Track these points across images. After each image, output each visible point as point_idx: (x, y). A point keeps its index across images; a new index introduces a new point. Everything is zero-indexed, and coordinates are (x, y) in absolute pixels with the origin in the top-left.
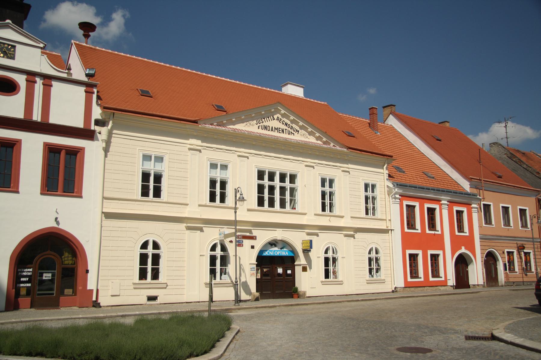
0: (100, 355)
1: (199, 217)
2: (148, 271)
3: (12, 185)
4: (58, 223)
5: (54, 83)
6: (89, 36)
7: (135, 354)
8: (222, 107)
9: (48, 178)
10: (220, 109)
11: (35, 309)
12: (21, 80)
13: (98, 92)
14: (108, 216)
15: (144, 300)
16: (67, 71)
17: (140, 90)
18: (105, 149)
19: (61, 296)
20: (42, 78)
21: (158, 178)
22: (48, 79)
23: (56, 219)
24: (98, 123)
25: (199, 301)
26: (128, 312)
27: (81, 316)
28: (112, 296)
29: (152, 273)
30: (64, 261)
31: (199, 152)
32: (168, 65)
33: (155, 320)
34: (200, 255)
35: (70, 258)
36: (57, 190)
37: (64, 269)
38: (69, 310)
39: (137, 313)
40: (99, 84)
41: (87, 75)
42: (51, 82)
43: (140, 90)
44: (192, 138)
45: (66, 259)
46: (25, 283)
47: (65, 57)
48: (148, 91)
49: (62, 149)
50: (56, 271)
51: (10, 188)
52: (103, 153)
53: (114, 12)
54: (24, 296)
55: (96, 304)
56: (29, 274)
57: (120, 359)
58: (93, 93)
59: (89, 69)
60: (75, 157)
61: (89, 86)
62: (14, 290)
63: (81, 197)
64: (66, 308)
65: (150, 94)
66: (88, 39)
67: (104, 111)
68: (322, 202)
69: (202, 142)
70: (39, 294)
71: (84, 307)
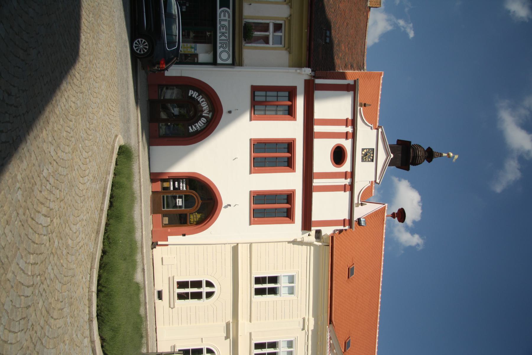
0: (107, 255)
1: (239, 334)
2: (185, 289)
3: (256, 168)
4: (226, 207)
5: (348, 193)
6: (394, 218)
7: (106, 286)
8: (353, 274)
9: (265, 196)
10: (347, 345)
11: (151, 195)
12: (346, 167)
13: (346, 230)
14: (235, 249)
15: (158, 288)
16: (360, 202)
17: (350, 339)
18: (295, 241)
19: (162, 215)
20: (350, 184)
21: (273, 291)
22: (351, 187)
23: (230, 205)
24: (318, 232)
25: (158, 340)
26: (147, 274)
27: (144, 233)
28: (162, 258)
29: (184, 293)
30: (193, 215)
31: (302, 328)
32: (381, 290)
33: (139, 301)
34: (202, 339)
35: (195, 220)
36: (255, 204)
37: (186, 215)
38: (149, 222)
39: (146, 283)
40: (352, 230)
41: (359, 220)
42: (348, 191)
43: (354, 267)
44: (315, 320)
45: (195, 216)
46: (173, 185)
47: (371, 199)
48: (350, 347)
49: (291, 205)
50: (183, 209)
51: (254, 167)
52: (292, 240)
53: (419, 236)
54: (162, 185)
55: (154, 245)
56: (181, 188)
57: (103, 273)
58: (344, 226)
59: (365, 220)
60: (287, 166)
61: (350, 221)
62: (167, 178)
63: (251, 173)
64: (151, 220)
65: (351, 276)
66: (391, 216)
67: (330, 237)
68: (265, 343)
69: (312, 331)
70: (163, 197)
71: (152, 235)
